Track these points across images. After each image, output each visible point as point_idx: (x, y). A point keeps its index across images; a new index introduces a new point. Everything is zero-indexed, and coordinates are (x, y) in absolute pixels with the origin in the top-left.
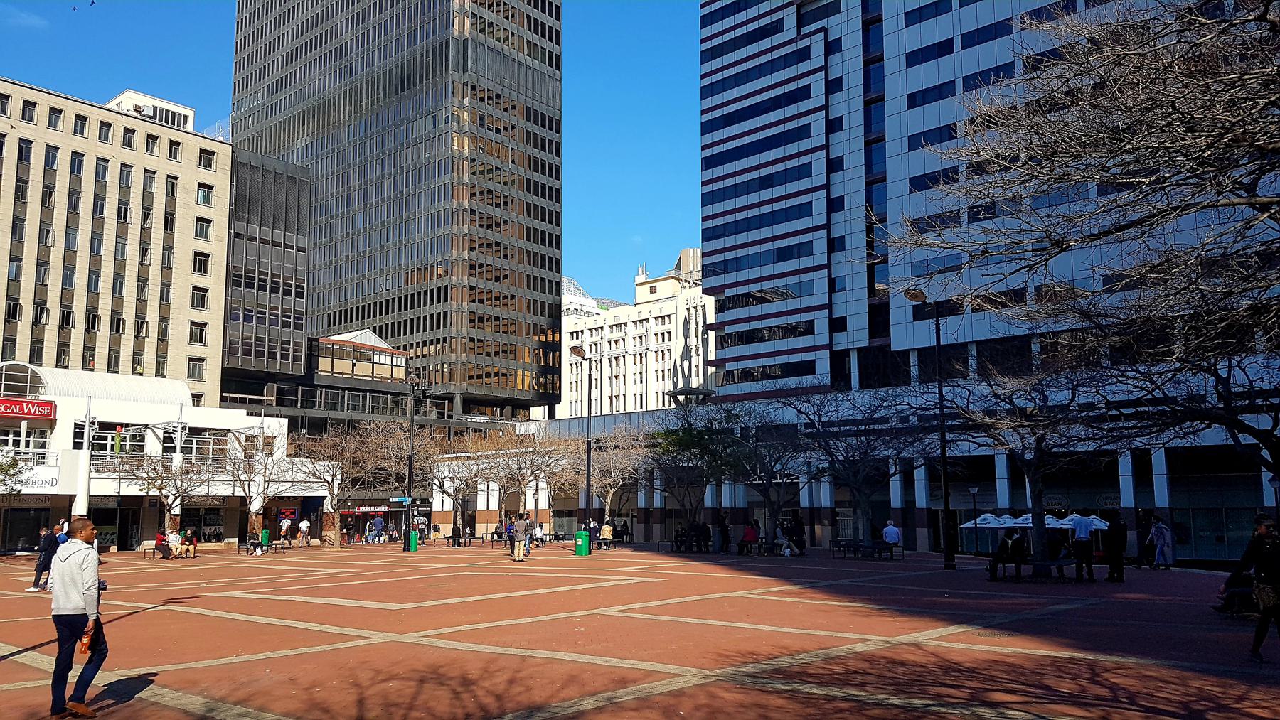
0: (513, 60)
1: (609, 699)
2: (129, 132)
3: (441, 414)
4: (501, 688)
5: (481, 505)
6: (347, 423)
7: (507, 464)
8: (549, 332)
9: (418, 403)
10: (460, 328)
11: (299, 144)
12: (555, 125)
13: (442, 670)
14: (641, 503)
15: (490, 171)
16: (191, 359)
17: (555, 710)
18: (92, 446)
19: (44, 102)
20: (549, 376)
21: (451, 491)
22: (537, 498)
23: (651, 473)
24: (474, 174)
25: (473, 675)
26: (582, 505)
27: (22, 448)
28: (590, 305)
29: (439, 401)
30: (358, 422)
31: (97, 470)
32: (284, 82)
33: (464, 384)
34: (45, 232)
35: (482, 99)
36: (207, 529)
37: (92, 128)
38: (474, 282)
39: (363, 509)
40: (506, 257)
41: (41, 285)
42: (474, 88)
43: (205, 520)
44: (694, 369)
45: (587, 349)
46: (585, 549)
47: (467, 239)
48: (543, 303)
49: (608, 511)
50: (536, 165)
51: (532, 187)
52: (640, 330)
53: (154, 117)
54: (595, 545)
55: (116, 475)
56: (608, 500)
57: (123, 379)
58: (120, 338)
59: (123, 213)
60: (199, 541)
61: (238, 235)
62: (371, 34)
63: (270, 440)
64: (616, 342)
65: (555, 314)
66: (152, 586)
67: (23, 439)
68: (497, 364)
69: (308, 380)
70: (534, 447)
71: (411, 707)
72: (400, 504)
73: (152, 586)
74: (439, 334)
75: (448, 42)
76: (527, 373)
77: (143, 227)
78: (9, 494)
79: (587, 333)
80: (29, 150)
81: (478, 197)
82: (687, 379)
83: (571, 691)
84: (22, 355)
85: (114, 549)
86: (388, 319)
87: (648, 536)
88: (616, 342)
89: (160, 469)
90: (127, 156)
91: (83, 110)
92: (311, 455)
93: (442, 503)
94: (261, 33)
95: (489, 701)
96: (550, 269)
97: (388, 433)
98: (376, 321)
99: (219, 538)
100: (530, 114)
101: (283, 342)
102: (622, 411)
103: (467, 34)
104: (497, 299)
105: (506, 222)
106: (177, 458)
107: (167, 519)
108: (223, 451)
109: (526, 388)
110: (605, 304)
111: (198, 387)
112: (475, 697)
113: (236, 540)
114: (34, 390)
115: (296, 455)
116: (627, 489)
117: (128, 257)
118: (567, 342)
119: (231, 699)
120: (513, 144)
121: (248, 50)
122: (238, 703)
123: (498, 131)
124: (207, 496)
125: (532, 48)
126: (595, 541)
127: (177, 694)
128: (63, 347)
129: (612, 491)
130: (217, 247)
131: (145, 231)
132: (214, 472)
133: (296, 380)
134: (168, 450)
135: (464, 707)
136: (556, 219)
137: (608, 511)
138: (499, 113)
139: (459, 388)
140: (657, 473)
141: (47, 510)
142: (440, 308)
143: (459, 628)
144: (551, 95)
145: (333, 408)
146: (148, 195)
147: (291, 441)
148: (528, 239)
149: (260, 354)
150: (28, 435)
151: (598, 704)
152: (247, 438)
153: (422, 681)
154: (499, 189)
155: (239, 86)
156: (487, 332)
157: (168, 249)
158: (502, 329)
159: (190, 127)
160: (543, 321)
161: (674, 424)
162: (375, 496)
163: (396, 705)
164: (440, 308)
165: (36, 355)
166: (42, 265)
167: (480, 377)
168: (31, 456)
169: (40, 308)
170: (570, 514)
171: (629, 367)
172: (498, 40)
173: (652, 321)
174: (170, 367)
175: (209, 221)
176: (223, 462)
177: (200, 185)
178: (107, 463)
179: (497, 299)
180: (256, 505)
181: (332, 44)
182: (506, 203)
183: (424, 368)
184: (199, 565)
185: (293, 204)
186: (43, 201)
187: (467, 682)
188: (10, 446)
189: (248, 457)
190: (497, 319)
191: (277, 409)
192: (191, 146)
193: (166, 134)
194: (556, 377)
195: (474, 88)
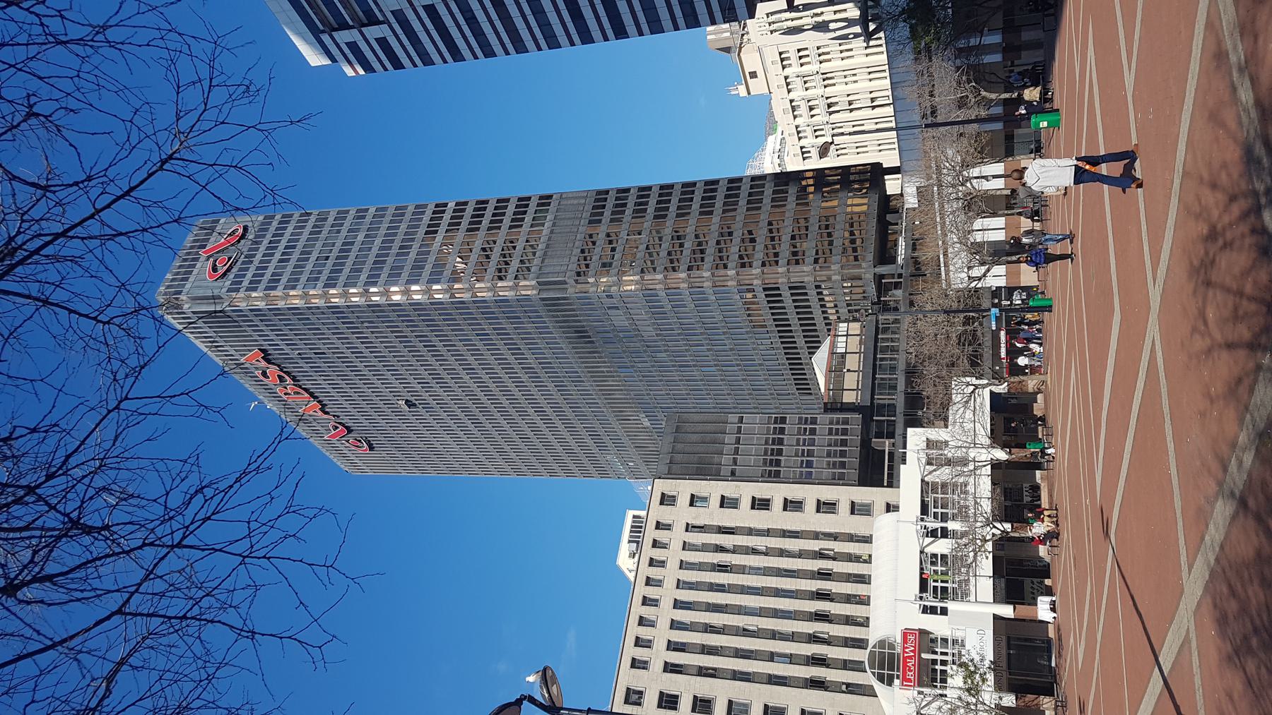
0: (549, 239)
1: (1241, 70)
2: (652, 563)
3: (897, 286)
4: (1221, 197)
5: (1000, 236)
6: (911, 373)
7: (953, 213)
8: (804, 183)
9: (886, 308)
10: (805, 273)
11: (647, 424)
12: (602, 195)
13: (1196, 263)
14: (997, 58)
15: (650, 255)
16: (852, 513)
17: (1252, 132)
18: (942, 599)
19: (634, 630)
20: (852, 178)
21: (983, 269)
22: (990, 176)
23: (960, 50)
24: (654, 269)
25: (1205, 229)
26: (999, 126)
27: (949, 658)
28: (772, 142)
29: (882, 286)
30: (908, 364)
31: (967, 595)
32: (595, 436)
33: (864, 265)
34: (745, 632)
35: (587, 266)
36: (1027, 499)
37: (652, 592)
38: (757, 263)
39: (1003, 354)
40: (730, 234)
41: (792, 637)
42: (578, 274)
43: (1016, 495)
44: (839, 16)
45: (821, 140)
46: (1052, 117)
47: (717, 273)
48: (774, 192)
49: (1007, 96)
50: (640, 211)
51: (660, 215)
52: (797, 84)
53: (638, 542)
54: (1047, 105)
55: (972, 579)
56: (993, 96)
57: (877, 571)
58: (837, 577)
59: (722, 568)
60: (1040, 506)
61: (733, 473)
62: (546, 365)
63: (930, 444)
64: (811, 109)
65: (784, 179)
66: (1089, 548)
67: (939, 657)
68: (841, 235)
69: (867, 411)
70: (933, 185)
71: (1240, 294)
72: (998, 319)
73: (1089, 548)
74: (812, 293)
75: (543, 299)
76: (850, 202)
77: (734, 552)
78: (994, 670)
79: (803, 142)
80: (677, 643)
81: (676, 264)
82: (850, 22)
83: (1229, 116)
84: (861, 655)
85: (1048, 582)
86: (801, 342)
87: (1036, 45)
88: (811, 109)
89: (965, 540)
90: (673, 564)
91: (637, 599)
92: (946, 404)
93: (997, 277)
94: (557, 459)
95: (1236, 210)
96: (739, 188)
97: (919, 336)
98: (804, 352)
99: (1036, 488)
100: (595, 221)
101: (830, 434)
102: (889, 93)
103: (534, 283)
104: (773, 239)
105: (697, 236)
106: (952, 525)
107: (1016, 535)
108: (944, 485)
109: (865, 201)
110: (771, 126)
111: (879, 506)
112: (1231, 225)
113: (1038, 473)
114: (892, 646)
115: (946, 419)
116: (979, 76)
117: (761, 565)
118: (815, 163)
119: (1220, 475)
120: (623, 235)
121: (572, 467)
122: (1225, 469)
123: (613, 250)
124: (992, 499)
125: (537, 222)
126: (1044, 105)
127: (1211, 526)
128: (849, 621)
129: (984, 93)
130: (746, 491)
131: (736, 550)
132: (966, 493)
133: (866, 422)
134: (945, 533)
135: (1243, 236)
136: (689, 187)
137: (1007, 96)
138: (598, 250)
139: (867, 270)
140: (962, 44)
141: (1009, 639)
142: (786, 294)
143: (1146, 248)
144: (576, 202)
145: (895, 388)
146: (704, 548)
147: (930, 424)
148: (499, 228)
149: (843, 454)
150: (936, 653)
151: (1247, 83)
152: (929, 463)
153: (1208, 284)
154: (666, 245)
155: (603, 474)
156: (808, 246)
157: (750, 532)
158: (803, 232)
159: (643, 513)
160: (792, 190)
161: (903, 30)
162: (989, 343)
163: (1236, 309)
164: (786, 294)
165: (860, 644)
166: (774, 635)
167: (855, 250)
168: (956, 651)
169: (814, 639)
170: (1009, 138)
171: (839, 90)
172: (534, 254)
173: (788, 71)
174: (863, 531)
175: (723, 497)
176: (955, 485)
177: (691, 504)
178: (960, 586)
179: (773, 239)
180: (1001, 455)
181: (558, 398)
182: (679, 237)
183: (848, 305)
184: (1065, 505)
185: (700, 427)
186: (719, 633)
187: (1213, 235)
188: (948, 668)
189: (949, 462)
190: (793, 237)
191: (898, 438)
192: (658, 513)
193: (651, 533)
194: (853, 170)
195: (578, 274)
